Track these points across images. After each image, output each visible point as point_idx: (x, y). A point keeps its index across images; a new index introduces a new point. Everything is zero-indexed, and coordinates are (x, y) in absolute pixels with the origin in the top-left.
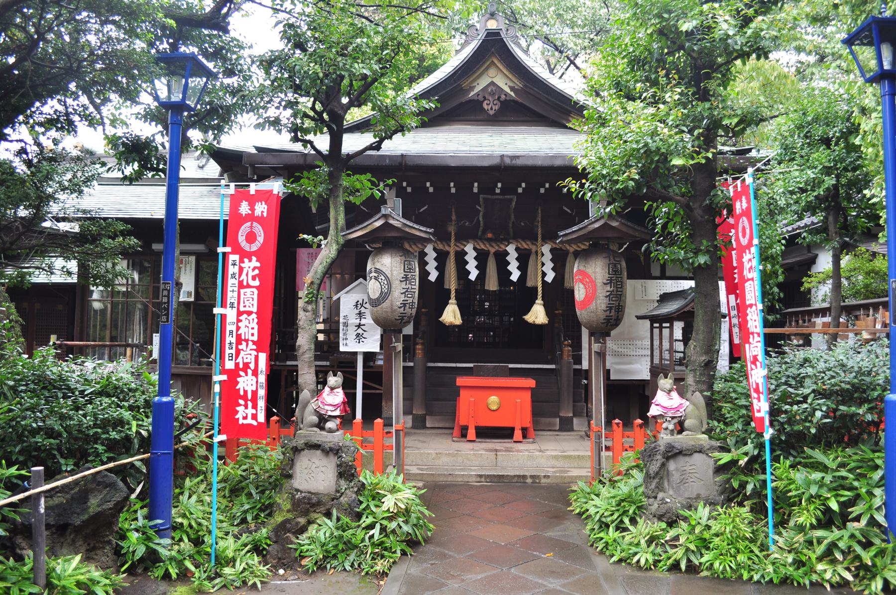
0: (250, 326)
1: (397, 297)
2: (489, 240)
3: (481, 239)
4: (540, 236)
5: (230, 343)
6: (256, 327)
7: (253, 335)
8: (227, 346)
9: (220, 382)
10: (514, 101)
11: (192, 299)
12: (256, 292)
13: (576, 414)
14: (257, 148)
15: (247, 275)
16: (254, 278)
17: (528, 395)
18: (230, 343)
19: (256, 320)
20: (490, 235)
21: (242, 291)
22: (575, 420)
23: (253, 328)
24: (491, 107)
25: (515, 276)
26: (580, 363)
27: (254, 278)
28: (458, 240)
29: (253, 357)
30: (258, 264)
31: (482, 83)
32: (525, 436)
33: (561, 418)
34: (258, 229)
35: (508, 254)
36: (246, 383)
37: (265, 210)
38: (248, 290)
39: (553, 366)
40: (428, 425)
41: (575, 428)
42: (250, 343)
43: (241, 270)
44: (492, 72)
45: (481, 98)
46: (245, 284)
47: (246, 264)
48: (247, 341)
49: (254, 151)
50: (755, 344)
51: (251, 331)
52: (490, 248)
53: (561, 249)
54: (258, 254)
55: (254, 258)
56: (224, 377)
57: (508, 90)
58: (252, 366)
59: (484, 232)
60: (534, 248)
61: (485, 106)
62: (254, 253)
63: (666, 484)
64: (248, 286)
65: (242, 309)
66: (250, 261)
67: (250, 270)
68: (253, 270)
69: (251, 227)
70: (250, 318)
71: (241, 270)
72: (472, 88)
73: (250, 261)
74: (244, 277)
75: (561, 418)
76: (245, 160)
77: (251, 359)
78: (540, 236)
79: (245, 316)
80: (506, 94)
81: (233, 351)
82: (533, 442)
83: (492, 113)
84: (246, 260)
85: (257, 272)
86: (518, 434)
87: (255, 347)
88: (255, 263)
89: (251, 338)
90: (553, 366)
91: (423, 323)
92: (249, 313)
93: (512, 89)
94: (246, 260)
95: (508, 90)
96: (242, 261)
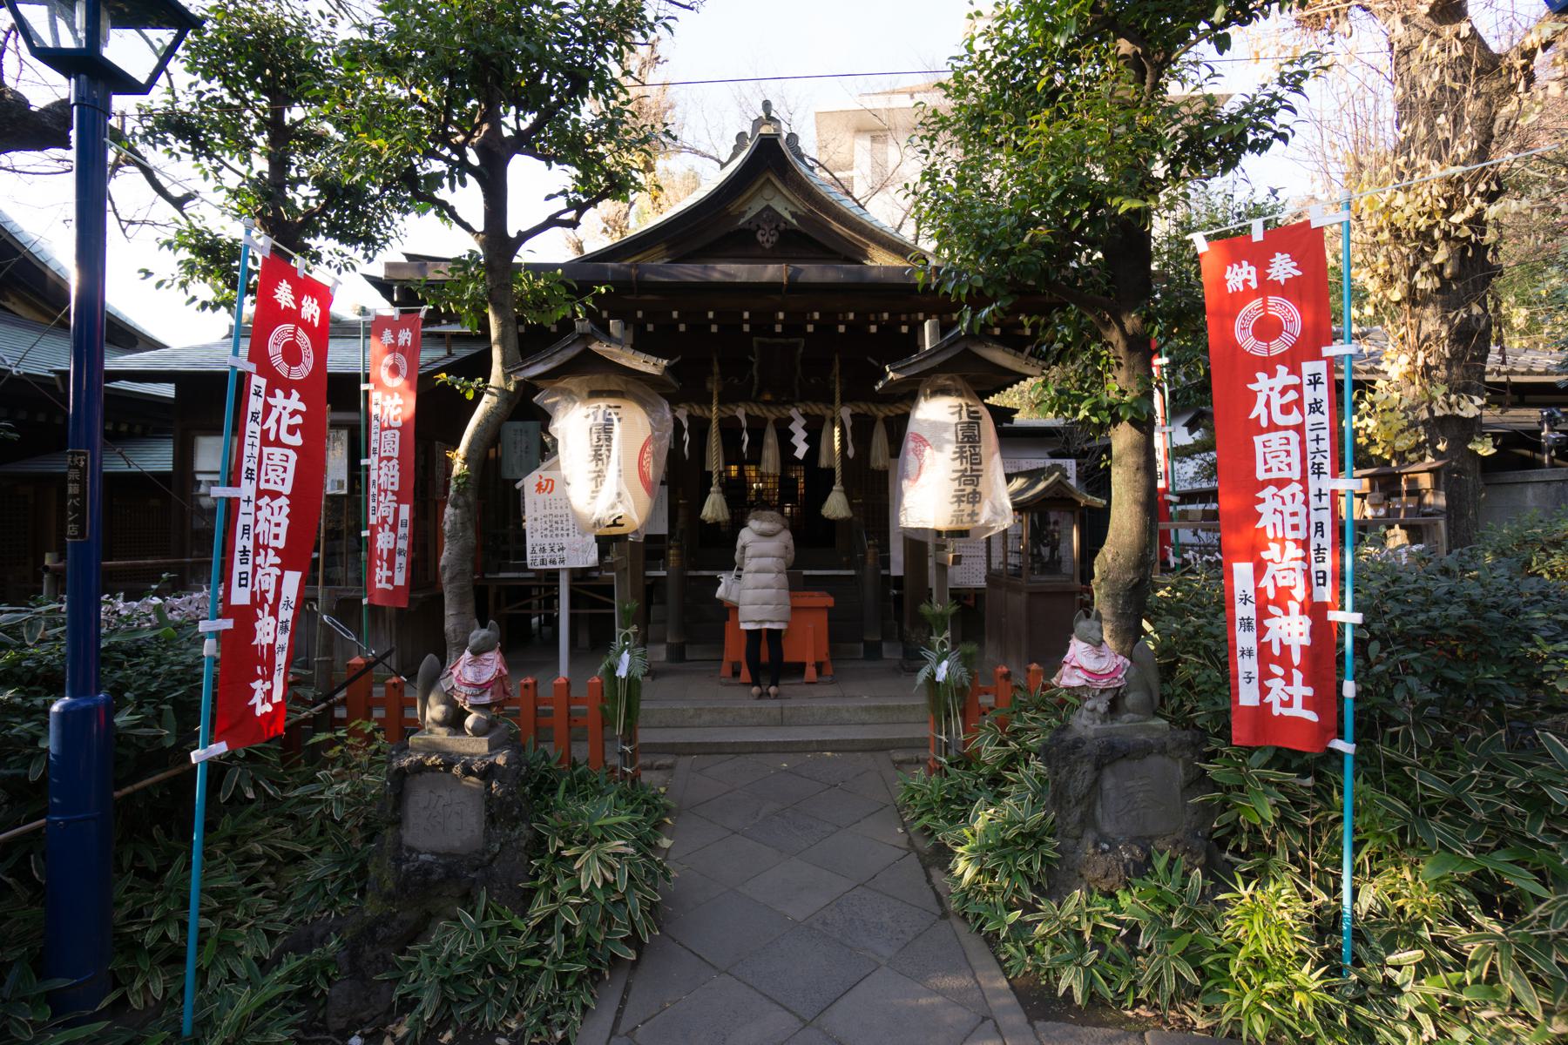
0: (274, 520)
1: (766, 526)
2: (767, 403)
3: (755, 402)
4: (838, 396)
5: (245, 552)
6: (285, 522)
7: (276, 537)
8: (237, 556)
9: (218, 635)
10: (796, 231)
11: (345, 492)
12: (293, 456)
13: (886, 637)
14: (408, 256)
15: (1268, 405)
16: (292, 430)
17: (824, 617)
18: (245, 552)
19: (286, 510)
20: (768, 397)
21: (266, 450)
22: (885, 646)
23: (278, 525)
24: (766, 238)
25: (801, 450)
26: (888, 567)
27: (292, 430)
28: (721, 402)
29: (273, 579)
30: (302, 407)
31: (756, 207)
32: (819, 673)
33: (866, 643)
34: (1281, 308)
35: (791, 420)
36: (266, 631)
37: (1253, 277)
38: (277, 451)
39: (852, 572)
40: (688, 657)
41: (886, 655)
42: (1290, 546)
43: (268, 409)
44: (768, 193)
45: (753, 227)
46: (272, 437)
47: (279, 399)
48: (266, 548)
49: (404, 260)
50: (268, 570)
51: (275, 530)
52: (768, 414)
53: (865, 415)
54: (304, 387)
55: (295, 395)
56: (228, 624)
57: (789, 217)
58: (270, 597)
59: (760, 392)
60: (829, 413)
61: (760, 238)
62: (297, 385)
63: (1099, 812)
64: (278, 443)
65: (263, 486)
66: (288, 396)
67: (286, 416)
68: (293, 414)
69: (1265, 306)
70: (276, 504)
71: (268, 409)
72: (743, 214)
73: (288, 396)
74: (271, 423)
75: (866, 643)
76: (585, 394)
77: (269, 584)
78: (838, 396)
79: (267, 499)
80: (786, 222)
81: (249, 568)
82: (832, 682)
83: (768, 246)
84: (279, 393)
85: (298, 420)
86: (810, 672)
87: (278, 560)
88: (295, 402)
89: (273, 543)
90: (852, 572)
91: (681, 519)
92: (275, 495)
93: (794, 215)
94: (279, 393)
95: (789, 217)
96: (270, 392)
